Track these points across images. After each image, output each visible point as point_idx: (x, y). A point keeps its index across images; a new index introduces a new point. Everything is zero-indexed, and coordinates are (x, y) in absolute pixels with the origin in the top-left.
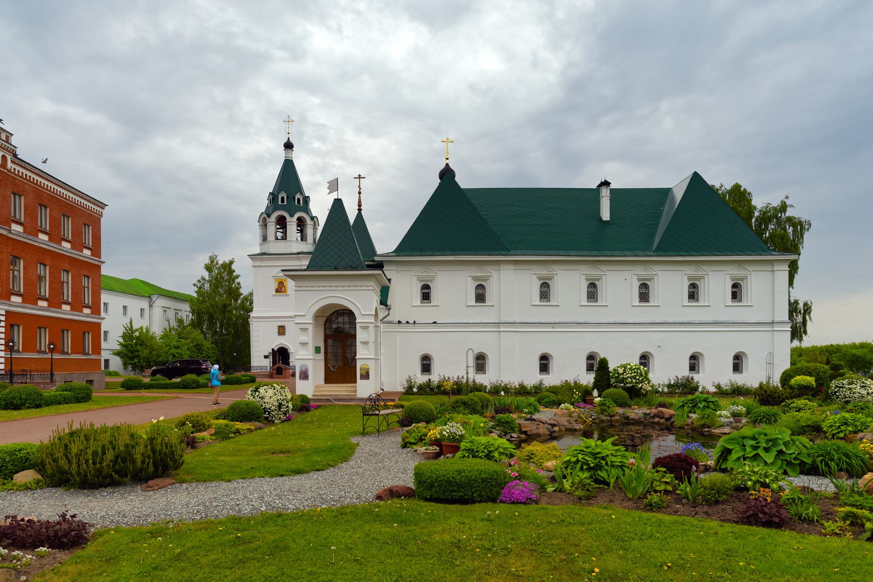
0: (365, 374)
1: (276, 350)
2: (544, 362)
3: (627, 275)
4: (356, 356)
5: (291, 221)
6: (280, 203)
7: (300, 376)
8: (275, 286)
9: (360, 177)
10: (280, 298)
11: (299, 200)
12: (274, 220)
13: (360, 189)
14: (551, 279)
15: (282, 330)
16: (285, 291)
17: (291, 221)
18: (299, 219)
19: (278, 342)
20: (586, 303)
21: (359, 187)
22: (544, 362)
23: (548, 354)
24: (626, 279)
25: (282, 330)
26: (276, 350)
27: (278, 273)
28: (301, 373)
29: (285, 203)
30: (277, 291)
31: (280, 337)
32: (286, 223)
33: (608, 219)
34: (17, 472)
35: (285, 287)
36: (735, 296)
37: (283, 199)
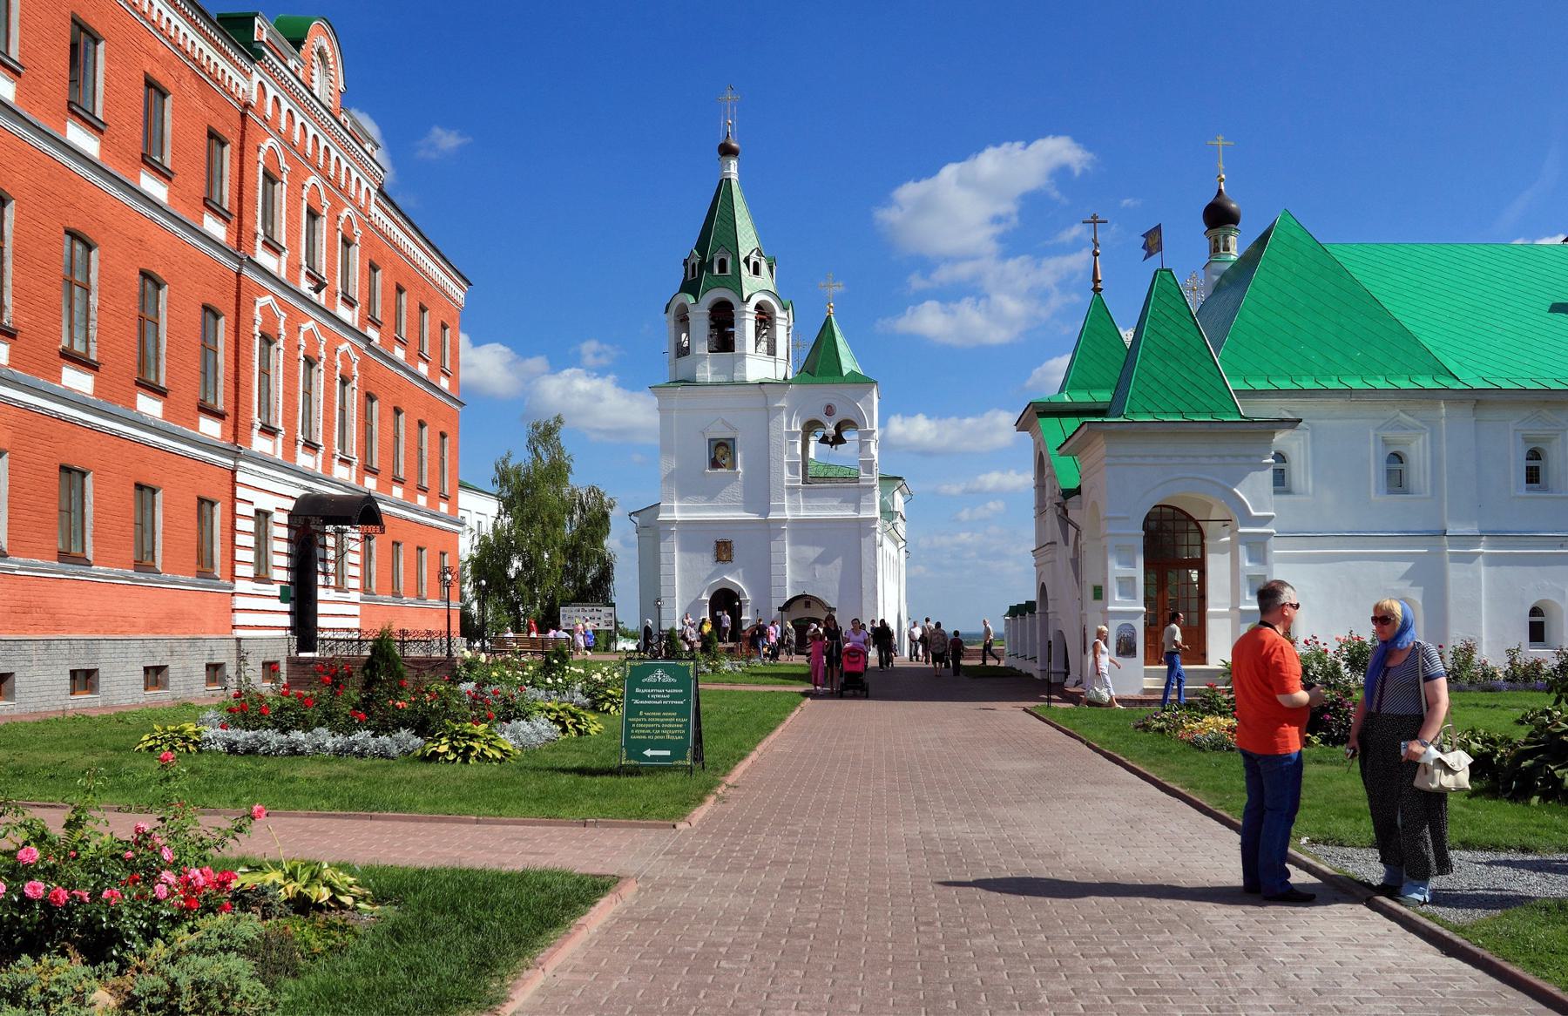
6: (716, 271)
7: (1118, 649)
9: (1095, 221)
13: (1097, 245)
20: (1523, 493)
21: (1094, 241)
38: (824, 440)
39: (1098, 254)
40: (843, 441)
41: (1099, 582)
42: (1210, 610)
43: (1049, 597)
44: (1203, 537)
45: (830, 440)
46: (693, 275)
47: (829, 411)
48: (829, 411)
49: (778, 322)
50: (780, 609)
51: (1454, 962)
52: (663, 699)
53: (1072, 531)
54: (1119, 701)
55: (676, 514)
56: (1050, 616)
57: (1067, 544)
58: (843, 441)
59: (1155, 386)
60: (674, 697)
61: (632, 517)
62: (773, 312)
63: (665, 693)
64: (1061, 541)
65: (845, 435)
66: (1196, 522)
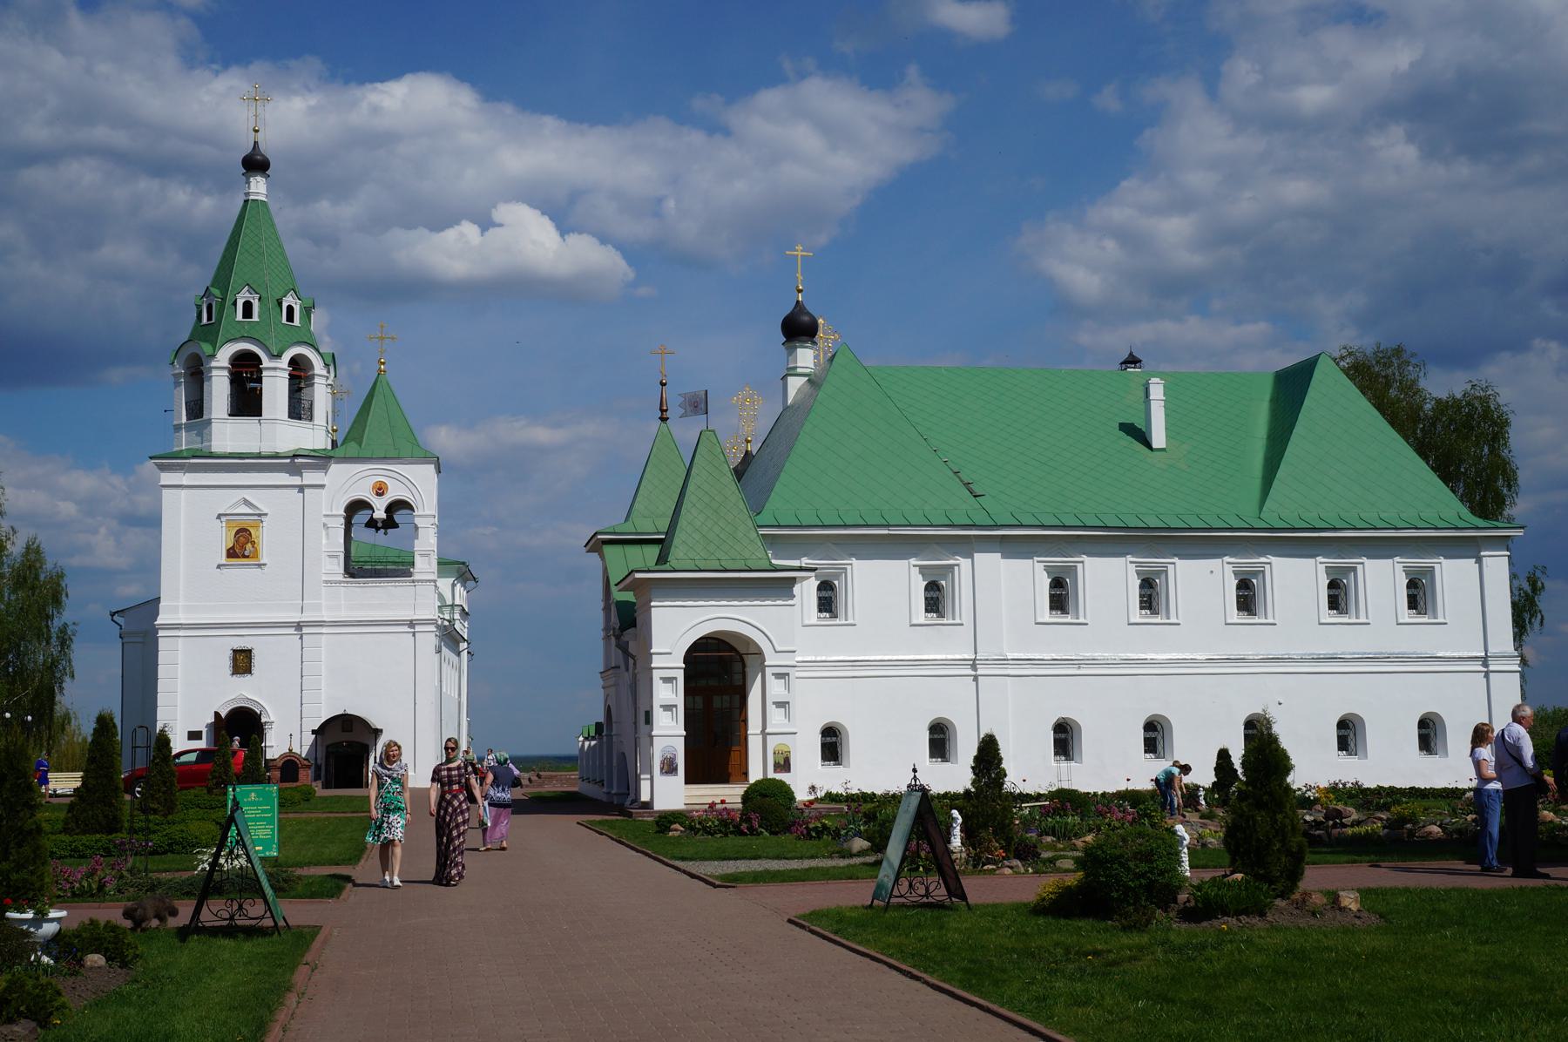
0: (782, 763)
1: (223, 715)
2: (1063, 736)
3: (1214, 563)
4: (652, 730)
5: (275, 369)
6: (239, 316)
7: (662, 769)
8: (222, 538)
10: (240, 574)
11: (290, 309)
12: (226, 364)
14: (837, 576)
15: (242, 662)
16: (255, 555)
17: (275, 369)
18: (295, 362)
19: (230, 693)
22: (1063, 736)
23: (830, 723)
24: (1212, 572)
25: (242, 662)
26: (223, 715)
27: (235, 505)
28: (663, 763)
29: (255, 318)
30: (231, 553)
31: (238, 679)
32: (260, 371)
33: (1163, 446)
34: (26, 1018)
35: (253, 543)
36: (1335, 603)
37: (248, 308)
38: (372, 523)
39: (665, 384)
40: (395, 526)
41: (648, 709)
42: (749, 732)
43: (613, 720)
44: (744, 666)
45: (380, 525)
46: (209, 318)
47: (380, 490)
48: (380, 490)
49: (317, 380)
50: (314, 732)
51: (639, 854)
52: (256, 814)
53: (631, 661)
54: (515, 760)
55: (181, 615)
56: (614, 739)
57: (627, 670)
58: (395, 526)
59: (697, 536)
60: (264, 811)
61: (116, 617)
62: (311, 366)
63: (258, 810)
64: (623, 667)
65: (397, 518)
66: (741, 656)
